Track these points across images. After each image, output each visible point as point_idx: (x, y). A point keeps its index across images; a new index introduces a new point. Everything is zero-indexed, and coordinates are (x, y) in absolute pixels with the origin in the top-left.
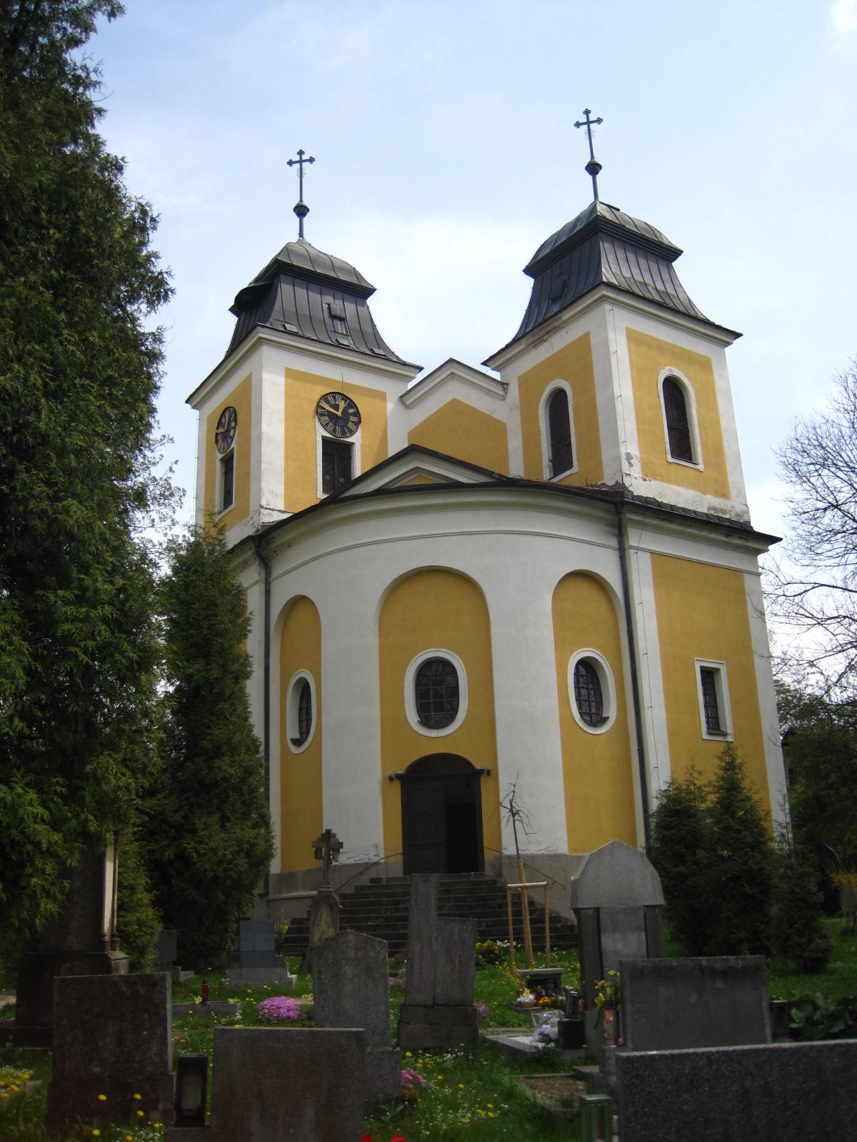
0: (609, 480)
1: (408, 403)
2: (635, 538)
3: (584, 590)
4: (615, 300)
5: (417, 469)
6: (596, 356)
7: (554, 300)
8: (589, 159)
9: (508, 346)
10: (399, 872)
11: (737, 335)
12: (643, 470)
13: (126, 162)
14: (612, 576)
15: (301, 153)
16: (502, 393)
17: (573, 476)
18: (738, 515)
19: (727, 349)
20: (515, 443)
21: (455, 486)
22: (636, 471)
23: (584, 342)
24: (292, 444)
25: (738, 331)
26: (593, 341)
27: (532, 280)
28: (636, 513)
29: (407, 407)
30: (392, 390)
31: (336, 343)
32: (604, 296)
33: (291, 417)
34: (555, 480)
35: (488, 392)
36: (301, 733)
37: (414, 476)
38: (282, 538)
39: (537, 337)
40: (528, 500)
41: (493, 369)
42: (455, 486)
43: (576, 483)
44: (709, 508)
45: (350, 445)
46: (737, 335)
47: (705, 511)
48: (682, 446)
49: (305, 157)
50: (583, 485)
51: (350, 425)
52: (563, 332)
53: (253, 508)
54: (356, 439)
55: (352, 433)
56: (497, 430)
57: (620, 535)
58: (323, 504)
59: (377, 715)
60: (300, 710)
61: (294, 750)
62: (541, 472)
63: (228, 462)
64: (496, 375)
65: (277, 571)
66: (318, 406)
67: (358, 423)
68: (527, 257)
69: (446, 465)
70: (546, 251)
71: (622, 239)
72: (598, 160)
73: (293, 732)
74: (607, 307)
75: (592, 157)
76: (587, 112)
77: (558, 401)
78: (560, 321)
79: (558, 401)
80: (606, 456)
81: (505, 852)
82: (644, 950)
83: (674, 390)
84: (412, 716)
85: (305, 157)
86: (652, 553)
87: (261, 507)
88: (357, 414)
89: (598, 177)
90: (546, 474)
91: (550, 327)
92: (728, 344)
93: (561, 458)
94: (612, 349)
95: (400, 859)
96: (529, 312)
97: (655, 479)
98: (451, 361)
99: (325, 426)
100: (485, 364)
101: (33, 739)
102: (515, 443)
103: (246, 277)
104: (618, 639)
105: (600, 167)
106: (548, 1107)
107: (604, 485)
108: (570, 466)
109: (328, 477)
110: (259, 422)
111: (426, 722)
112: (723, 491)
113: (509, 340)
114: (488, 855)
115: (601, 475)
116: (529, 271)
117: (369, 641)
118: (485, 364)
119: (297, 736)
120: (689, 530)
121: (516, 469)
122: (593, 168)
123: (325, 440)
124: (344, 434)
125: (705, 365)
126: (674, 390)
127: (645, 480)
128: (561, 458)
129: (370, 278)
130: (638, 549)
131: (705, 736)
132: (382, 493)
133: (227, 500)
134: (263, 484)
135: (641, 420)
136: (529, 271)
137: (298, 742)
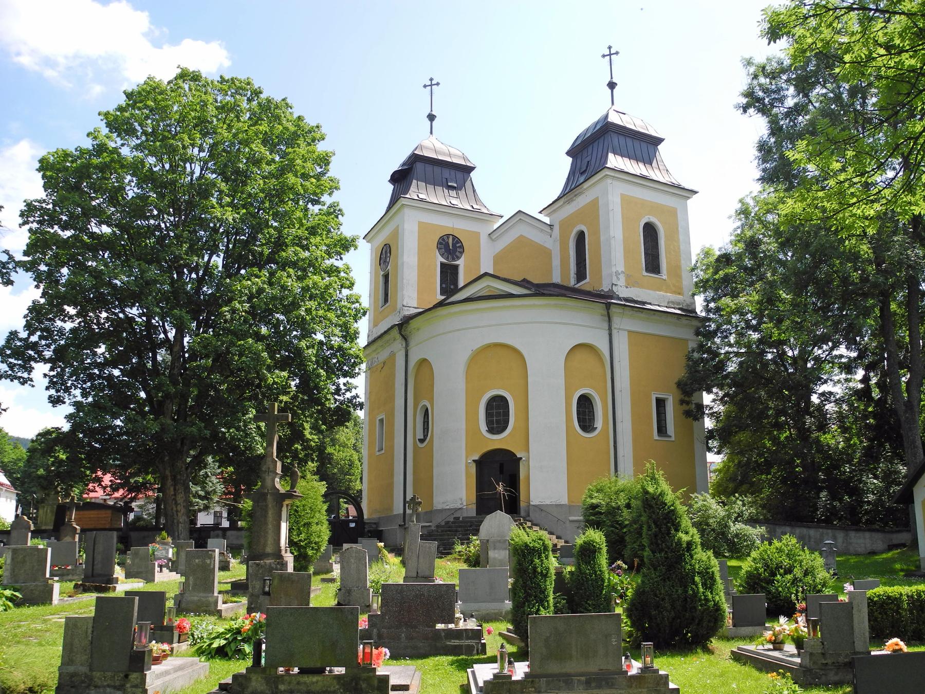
0: (605, 288)
1: (493, 238)
2: (617, 322)
6: (601, 212)
7: (582, 173)
8: (609, 79)
9: (554, 202)
10: (473, 513)
11: (696, 192)
12: (626, 281)
14: (604, 348)
15: (431, 80)
16: (550, 231)
17: (584, 285)
19: (689, 201)
20: (556, 262)
21: (511, 296)
22: (622, 281)
23: (595, 202)
24: (421, 266)
25: (695, 189)
26: (601, 202)
27: (571, 159)
29: (493, 240)
31: (450, 205)
32: (607, 175)
33: (421, 252)
34: (577, 286)
35: (542, 230)
36: (424, 436)
38: (414, 324)
42: (511, 296)
45: (456, 267)
46: (696, 192)
48: (653, 265)
49: (434, 82)
50: (591, 290)
51: (457, 254)
52: (584, 196)
53: (399, 306)
54: (461, 262)
55: (458, 258)
58: (441, 304)
59: (464, 427)
60: (424, 422)
61: (420, 445)
62: (569, 280)
63: (386, 277)
64: (547, 220)
65: (412, 343)
66: (448, 235)
67: (462, 253)
68: (568, 146)
70: (579, 142)
71: (599, 156)
72: (614, 80)
74: (609, 181)
75: (612, 78)
76: (431, 80)
77: (581, 238)
79: (581, 238)
80: (605, 272)
81: (531, 503)
83: (650, 231)
84: (483, 427)
85: (434, 82)
86: (629, 331)
87: (403, 306)
88: (462, 247)
89: (614, 90)
90: (572, 282)
91: (577, 192)
92: (689, 198)
93: (581, 274)
94: (611, 208)
95: (474, 507)
96: (568, 179)
97: (634, 286)
98: (520, 211)
99: (442, 255)
100: (540, 212)
102: (556, 262)
103: (396, 164)
104: (606, 382)
105: (616, 84)
106: (779, 530)
108: (586, 278)
109: (444, 286)
110: (403, 255)
111: (491, 430)
113: (556, 198)
114: (523, 504)
115: (601, 284)
116: (569, 153)
117: (460, 385)
119: (422, 437)
121: (556, 279)
123: (442, 264)
124: (454, 259)
125: (673, 213)
126: (650, 231)
127: (627, 287)
128: (581, 274)
129: (473, 161)
131: (656, 437)
132: (468, 300)
133: (386, 300)
134: (405, 292)
136: (569, 153)
137: (422, 441)
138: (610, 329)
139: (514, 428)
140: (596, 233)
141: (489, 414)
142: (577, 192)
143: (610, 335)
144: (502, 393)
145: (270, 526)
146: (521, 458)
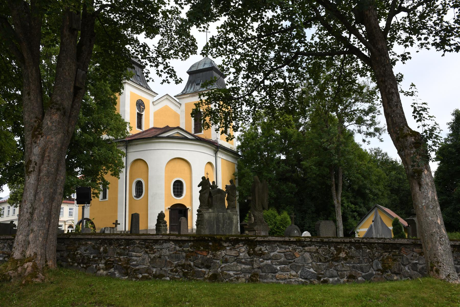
2: (219, 155)
3: (209, 166)
5: (178, 132)
13: (413, 115)
21: (186, 139)
24: (131, 113)
27: (188, 75)
28: (221, 149)
30: (151, 99)
35: (176, 105)
37: (232, 155)
43: (202, 137)
47: (229, 148)
56: (177, 116)
57: (216, 153)
69: (185, 133)
73: (134, 194)
100: (175, 96)
107: (212, 140)
117: (162, 173)
118: (175, 96)
123: (138, 113)
130: (220, 157)
132: (168, 137)
143: (216, 159)
146: (188, 208)
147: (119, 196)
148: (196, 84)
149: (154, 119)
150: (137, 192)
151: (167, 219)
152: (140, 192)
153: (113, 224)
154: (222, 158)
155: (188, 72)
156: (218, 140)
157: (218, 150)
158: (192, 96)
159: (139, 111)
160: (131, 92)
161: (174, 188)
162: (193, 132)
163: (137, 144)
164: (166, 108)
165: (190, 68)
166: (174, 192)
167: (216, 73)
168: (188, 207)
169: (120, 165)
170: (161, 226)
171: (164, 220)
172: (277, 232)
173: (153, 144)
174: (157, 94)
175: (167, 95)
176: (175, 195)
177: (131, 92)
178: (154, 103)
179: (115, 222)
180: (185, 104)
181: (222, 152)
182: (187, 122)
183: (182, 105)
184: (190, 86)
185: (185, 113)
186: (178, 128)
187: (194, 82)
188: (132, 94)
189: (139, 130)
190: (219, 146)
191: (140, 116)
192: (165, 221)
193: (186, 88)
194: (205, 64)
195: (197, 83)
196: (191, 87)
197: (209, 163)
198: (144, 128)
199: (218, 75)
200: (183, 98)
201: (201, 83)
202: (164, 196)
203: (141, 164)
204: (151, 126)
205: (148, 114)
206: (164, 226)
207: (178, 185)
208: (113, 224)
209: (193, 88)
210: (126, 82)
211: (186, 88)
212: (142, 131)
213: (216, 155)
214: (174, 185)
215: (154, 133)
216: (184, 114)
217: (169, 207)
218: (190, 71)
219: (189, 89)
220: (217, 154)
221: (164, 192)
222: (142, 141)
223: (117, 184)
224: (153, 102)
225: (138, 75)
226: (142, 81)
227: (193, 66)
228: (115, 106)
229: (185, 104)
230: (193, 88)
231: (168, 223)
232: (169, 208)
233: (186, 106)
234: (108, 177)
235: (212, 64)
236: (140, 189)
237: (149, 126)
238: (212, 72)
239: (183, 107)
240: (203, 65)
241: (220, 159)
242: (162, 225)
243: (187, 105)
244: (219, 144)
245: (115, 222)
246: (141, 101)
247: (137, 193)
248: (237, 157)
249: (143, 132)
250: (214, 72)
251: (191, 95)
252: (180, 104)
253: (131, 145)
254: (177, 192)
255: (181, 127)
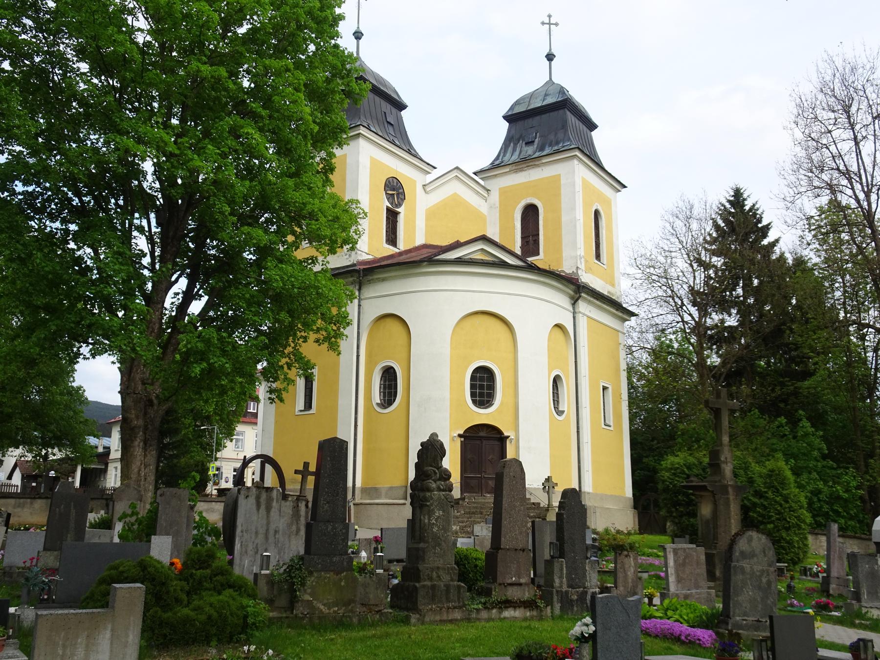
1: (428, 190)
2: (582, 306)
3: (558, 333)
4: (581, 159)
5: (482, 250)
8: (548, 51)
16: (486, 196)
18: (618, 298)
21: (503, 265)
25: (436, 166)
27: (508, 124)
32: (576, 155)
33: (372, 192)
35: (478, 193)
39: (519, 167)
40: (542, 279)
41: (481, 178)
42: (503, 265)
44: (609, 292)
45: (397, 213)
47: (606, 293)
56: (480, 217)
57: (575, 302)
68: (505, 110)
73: (377, 398)
74: (576, 162)
75: (550, 50)
78: (540, 162)
82: (637, 527)
92: (620, 191)
100: (475, 173)
101: (253, 596)
107: (563, 271)
112: (613, 285)
117: (446, 349)
118: (475, 173)
120: (605, 306)
122: (550, 57)
123: (388, 209)
130: (584, 314)
132: (459, 261)
135: (585, 237)
138: (574, 313)
139: (502, 403)
140: (556, 210)
141: (492, 387)
142: (531, 164)
143: (574, 318)
144: (557, 373)
145: (733, 521)
146: (508, 437)
147: (341, 402)
148: (526, 144)
149: (426, 226)
150: (384, 393)
151: (451, 462)
152: (390, 394)
153: (296, 472)
154: (588, 317)
155: (506, 118)
156: (580, 272)
157: (580, 296)
158: (516, 171)
159: (392, 204)
160: (372, 159)
161: (473, 387)
162: (518, 251)
163: (384, 280)
164: (455, 201)
165: (512, 108)
166: (473, 395)
167: (573, 117)
168: (506, 434)
169: (343, 320)
170: (429, 490)
171: (440, 467)
172: (755, 505)
173: (422, 279)
174: (435, 168)
175: (457, 168)
176: (474, 402)
177: (372, 159)
178: (426, 187)
179: (301, 468)
180: (500, 189)
181: (589, 302)
182: (505, 228)
183: (492, 192)
184: (510, 149)
185: (500, 211)
186: (484, 238)
187: (521, 137)
188: (374, 162)
189: (391, 247)
190: (583, 287)
191: (392, 216)
192: (446, 470)
193: (502, 154)
194: (546, 95)
195: (527, 140)
196: (514, 150)
197: (558, 326)
198: (403, 244)
199: (577, 121)
200: (495, 176)
201: (537, 140)
202: (448, 403)
203: (394, 327)
204: (420, 241)
205: (413, 210)
206: (439, 490)
207: (482, 379)
208: (296, 472)
209: (517, 153)
210: (359, 134)
211: (502, 154)
212: (398, 251)
213: (574, 308)
214: (473, 378)
215: (425, 253)
216: (498, 214)
217: (462, 432)
218: (510, 113)
219: (508, 155)
220: (576, 306)
221: (447, 394)
222: (396, 270)
223: (335, 369)
224: (424, 186)
225: (389, 123)
226: (398, 135)
227: (517, 103)
228: (330, 176)
229: (500, 189)
230: (517, 153)
231: (456, 479)
232: (460, 436)
233: (500, 195)
234: (310, 349)
235: (564, 93)
236: (390, 387)
237: (415, 242)
238: (565, 114)
239: (495, 197)
240: (541, 98)
241: (585, 317)
242: (434, 485)
243: (503, 192)
244: (582, 282)
245: (301, 468)
246: (395, 181)
247: (384, 397)
248: (625, 317)
249: (400, 254)
250: (568, 113)
251: (514, 168)
252: (488, 190)
253: (370, 282)
254: (481, 395)
255: (489, 235)
